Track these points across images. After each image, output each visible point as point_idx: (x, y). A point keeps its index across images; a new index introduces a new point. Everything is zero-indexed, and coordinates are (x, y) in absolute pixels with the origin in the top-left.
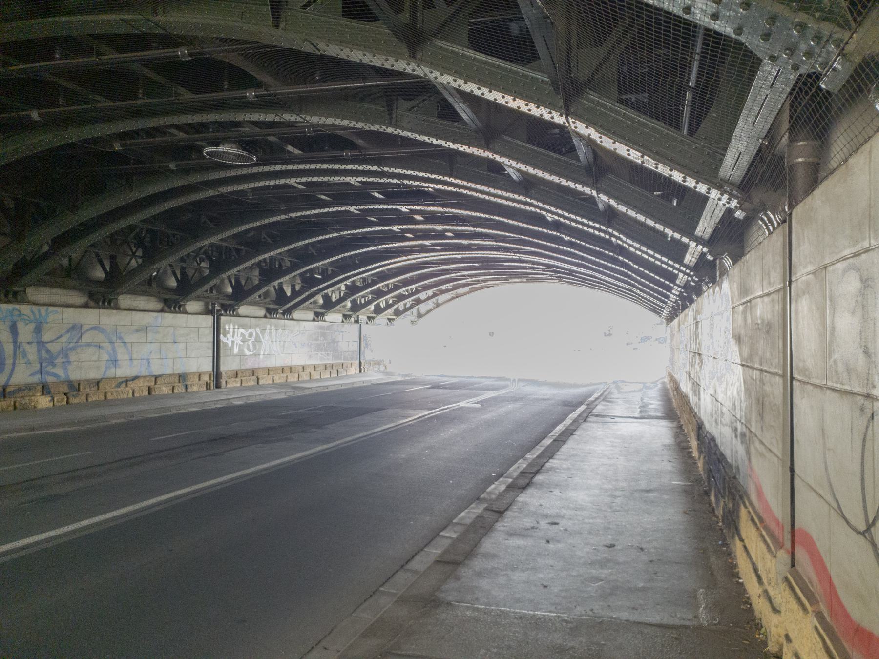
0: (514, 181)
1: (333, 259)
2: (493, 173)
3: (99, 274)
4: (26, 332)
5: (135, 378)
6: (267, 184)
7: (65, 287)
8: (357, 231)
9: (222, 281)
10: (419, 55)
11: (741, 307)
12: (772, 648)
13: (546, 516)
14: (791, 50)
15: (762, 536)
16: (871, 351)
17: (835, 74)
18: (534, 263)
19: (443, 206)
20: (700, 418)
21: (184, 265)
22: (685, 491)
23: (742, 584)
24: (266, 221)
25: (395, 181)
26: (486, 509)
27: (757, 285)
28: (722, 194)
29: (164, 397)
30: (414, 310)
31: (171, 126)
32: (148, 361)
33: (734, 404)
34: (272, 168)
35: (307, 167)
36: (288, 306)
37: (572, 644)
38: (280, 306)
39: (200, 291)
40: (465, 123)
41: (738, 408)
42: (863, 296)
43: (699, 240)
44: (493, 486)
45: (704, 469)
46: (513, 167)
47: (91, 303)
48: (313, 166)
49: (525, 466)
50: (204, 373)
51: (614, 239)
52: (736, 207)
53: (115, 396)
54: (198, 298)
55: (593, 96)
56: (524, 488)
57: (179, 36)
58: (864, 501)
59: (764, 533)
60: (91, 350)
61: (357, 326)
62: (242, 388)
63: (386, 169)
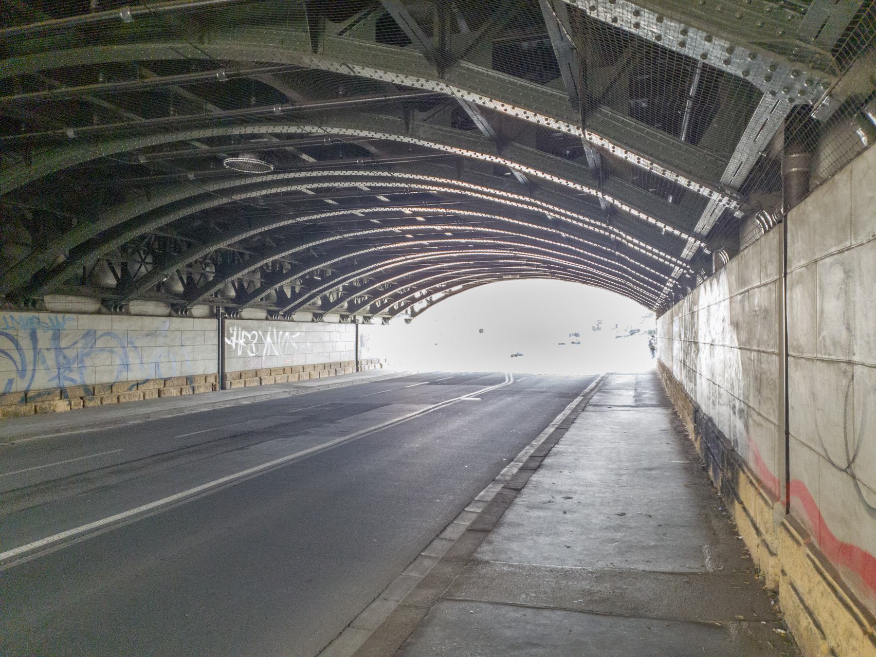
0: (520, 183)
1: (335, 261)
2: (499, 176)
3: (111, 281)
4: (44, 338)
5: (146, 381)
6: (279, 191)
7: (78, 294)
8: (359, 233)
9: (226, 286)
10: (447, 76)
11: (739, 297)
12: (770, 585)
13: (560, 492)
14: (788, 89)
15: (760, 494)
16: (852, 326)
17: (823, 106)
18: (529, 259)
19: (446, 207)
20: (696, 403)
21: (189, 269)
22: (685, 468)
23: (742, 540)
24: (274, 226)
25: (403, 185)
26: (503, 488)
27: (755, 277)
28: (723, 197)
29: (174, 399)
30: (409, 309)
31: (197, 140)
32: (157, 364)
33: (732, 385)
34: (286, 176)
35: (320, 174)
36: (288, 308)
37: (599, 588)
38: (281, 309)
39: (206, 295)
40: (480, 132)
41: (736, 387)
42: (846, 284)
43: (697, 236)
44: (505, 469)
45: (701, 448)
46: (520, 170)
47: (104, 310)
48: (325, 173)
49: (532, 451)
50: (210, 375)
51: (613, 236)
52: (735, 207)
53: (127, 399)
54: (204, 302)
55: (606, 110)
56: (535, 470)
57: (221, 61)
58: (846, 445)
59: (762, 491)
60: (105, 355)
61: (354, 325)
62: (246, 389)
63: (396, 175)
